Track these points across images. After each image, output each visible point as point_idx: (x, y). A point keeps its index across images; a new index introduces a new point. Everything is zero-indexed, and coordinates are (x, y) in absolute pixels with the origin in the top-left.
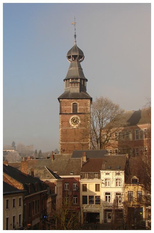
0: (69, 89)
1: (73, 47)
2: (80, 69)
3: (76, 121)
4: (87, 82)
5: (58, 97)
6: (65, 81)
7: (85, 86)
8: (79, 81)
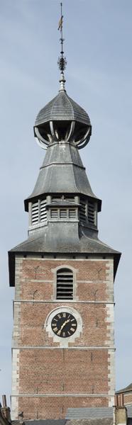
0: (42, 203)
1: (54, 99)
2: (78, 167)
3: (68, 326)
4: (98, 213)
5: (9, 250)
6: (30, 204)
7: (95, 224)
8: (76, 201)
